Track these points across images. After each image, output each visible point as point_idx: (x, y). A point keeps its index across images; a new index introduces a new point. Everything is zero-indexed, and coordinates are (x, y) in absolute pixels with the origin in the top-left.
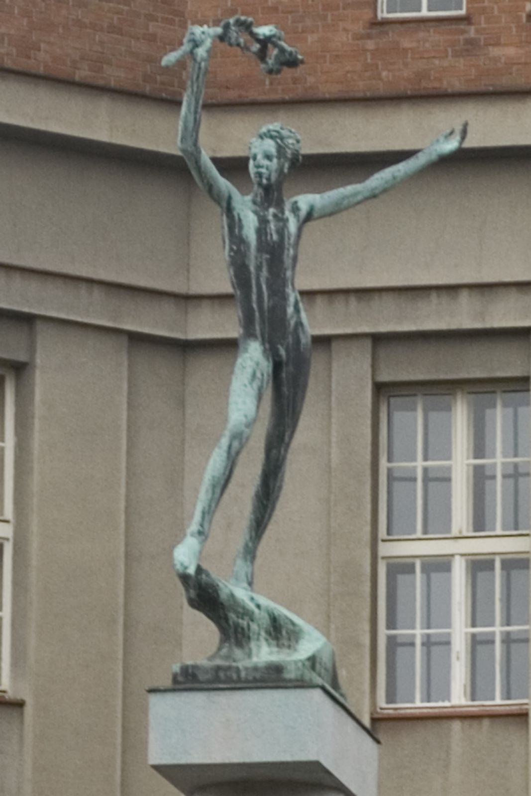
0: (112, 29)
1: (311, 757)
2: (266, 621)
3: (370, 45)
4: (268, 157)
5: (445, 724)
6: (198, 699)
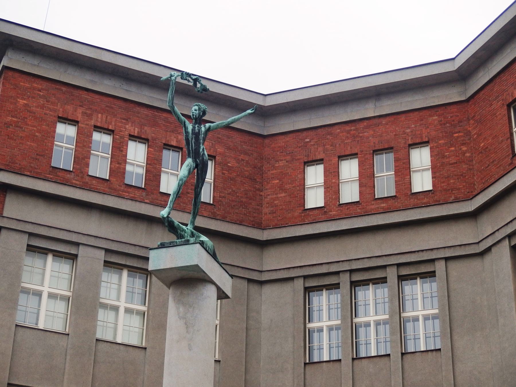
0: (245, 214)
1: (196, 263)
2: (190, 233)
3: (303, 215)
4: (196, 110)
5: (322, 364)
6: (164, 250)
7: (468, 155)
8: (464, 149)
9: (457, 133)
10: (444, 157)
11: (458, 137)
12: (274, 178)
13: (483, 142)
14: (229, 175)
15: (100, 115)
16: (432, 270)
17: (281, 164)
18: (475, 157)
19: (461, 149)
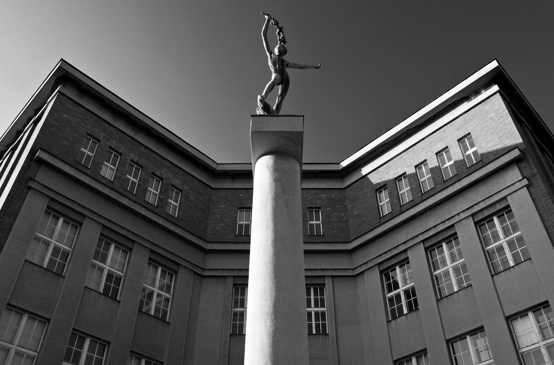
8: (343, 215)
15: (115, 142)
16: (323, 282)
17: (223, 206)
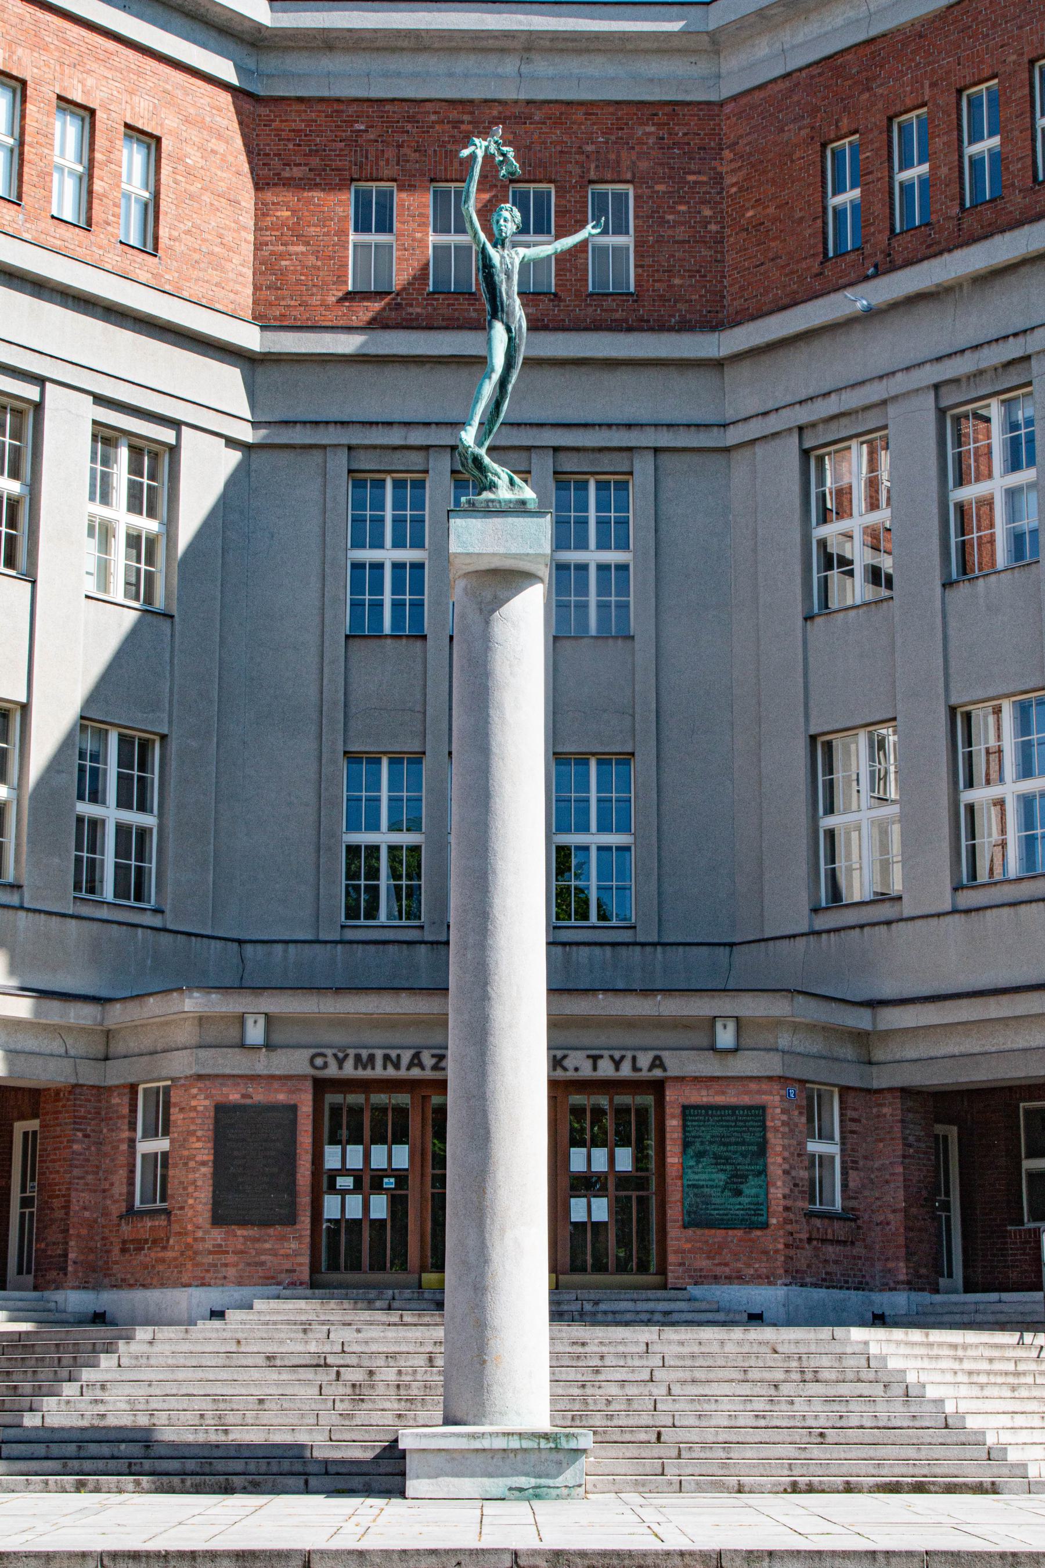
7: (713, 227)
9: (694, 173)
10: (662, 222)
11: (695, 182)
12: (278, 204)
13: (753, 207)
14: (188, 186)
18: (729, 236)
19: (699, 212)
